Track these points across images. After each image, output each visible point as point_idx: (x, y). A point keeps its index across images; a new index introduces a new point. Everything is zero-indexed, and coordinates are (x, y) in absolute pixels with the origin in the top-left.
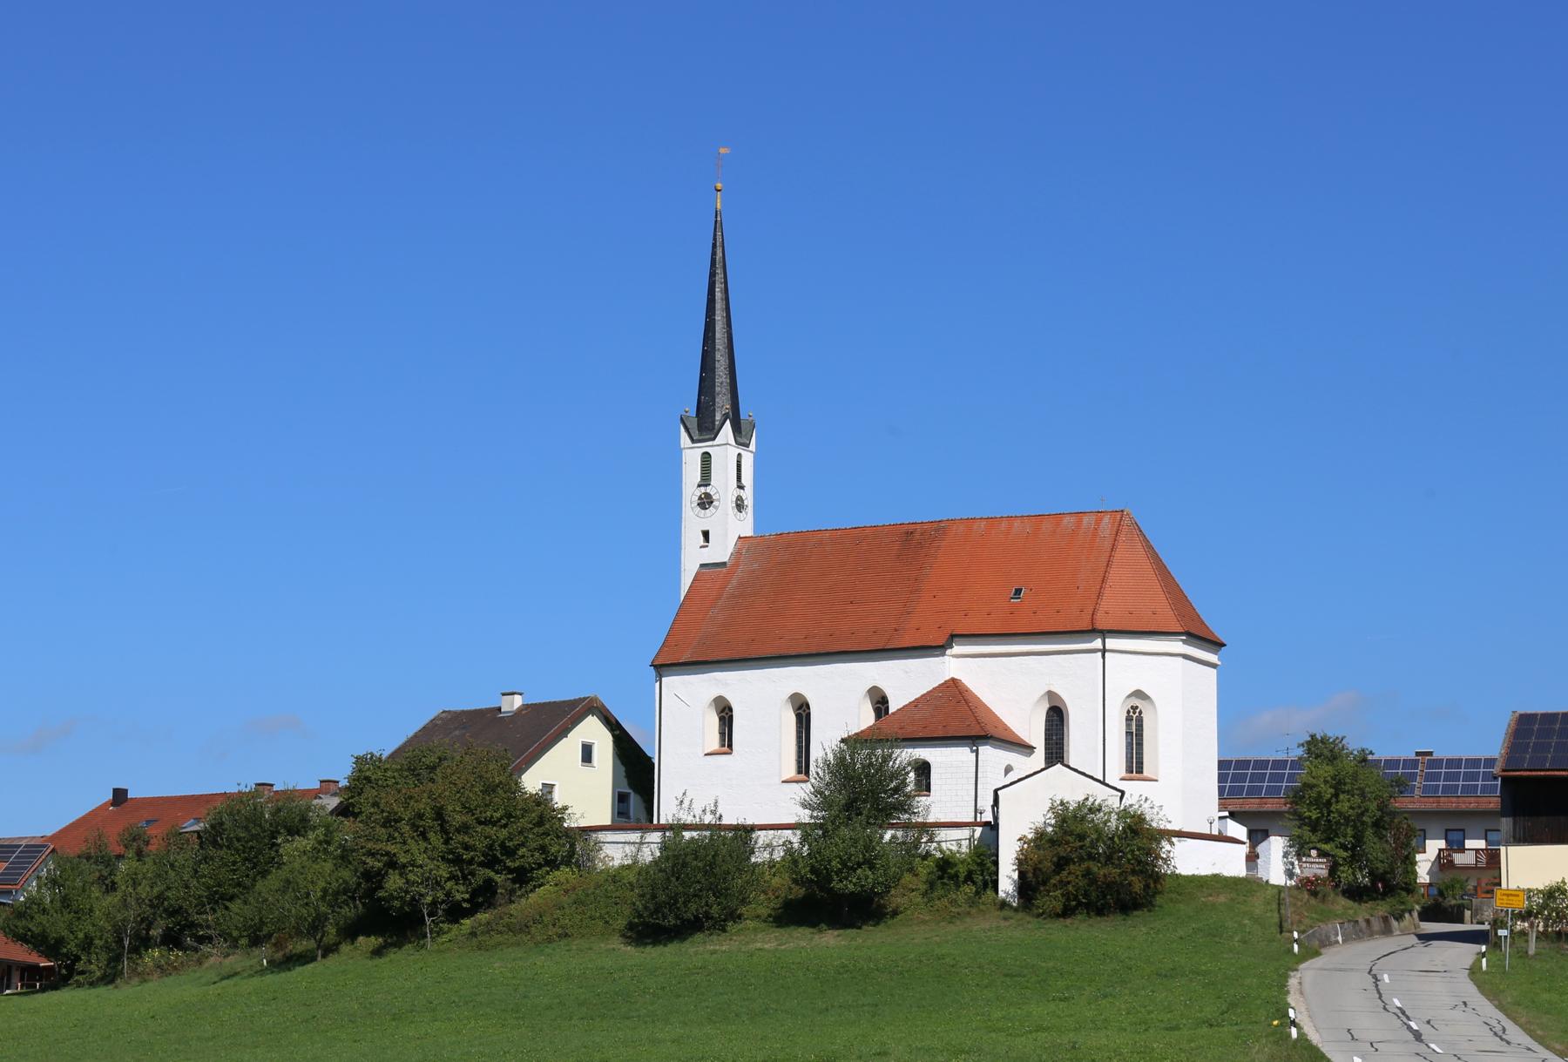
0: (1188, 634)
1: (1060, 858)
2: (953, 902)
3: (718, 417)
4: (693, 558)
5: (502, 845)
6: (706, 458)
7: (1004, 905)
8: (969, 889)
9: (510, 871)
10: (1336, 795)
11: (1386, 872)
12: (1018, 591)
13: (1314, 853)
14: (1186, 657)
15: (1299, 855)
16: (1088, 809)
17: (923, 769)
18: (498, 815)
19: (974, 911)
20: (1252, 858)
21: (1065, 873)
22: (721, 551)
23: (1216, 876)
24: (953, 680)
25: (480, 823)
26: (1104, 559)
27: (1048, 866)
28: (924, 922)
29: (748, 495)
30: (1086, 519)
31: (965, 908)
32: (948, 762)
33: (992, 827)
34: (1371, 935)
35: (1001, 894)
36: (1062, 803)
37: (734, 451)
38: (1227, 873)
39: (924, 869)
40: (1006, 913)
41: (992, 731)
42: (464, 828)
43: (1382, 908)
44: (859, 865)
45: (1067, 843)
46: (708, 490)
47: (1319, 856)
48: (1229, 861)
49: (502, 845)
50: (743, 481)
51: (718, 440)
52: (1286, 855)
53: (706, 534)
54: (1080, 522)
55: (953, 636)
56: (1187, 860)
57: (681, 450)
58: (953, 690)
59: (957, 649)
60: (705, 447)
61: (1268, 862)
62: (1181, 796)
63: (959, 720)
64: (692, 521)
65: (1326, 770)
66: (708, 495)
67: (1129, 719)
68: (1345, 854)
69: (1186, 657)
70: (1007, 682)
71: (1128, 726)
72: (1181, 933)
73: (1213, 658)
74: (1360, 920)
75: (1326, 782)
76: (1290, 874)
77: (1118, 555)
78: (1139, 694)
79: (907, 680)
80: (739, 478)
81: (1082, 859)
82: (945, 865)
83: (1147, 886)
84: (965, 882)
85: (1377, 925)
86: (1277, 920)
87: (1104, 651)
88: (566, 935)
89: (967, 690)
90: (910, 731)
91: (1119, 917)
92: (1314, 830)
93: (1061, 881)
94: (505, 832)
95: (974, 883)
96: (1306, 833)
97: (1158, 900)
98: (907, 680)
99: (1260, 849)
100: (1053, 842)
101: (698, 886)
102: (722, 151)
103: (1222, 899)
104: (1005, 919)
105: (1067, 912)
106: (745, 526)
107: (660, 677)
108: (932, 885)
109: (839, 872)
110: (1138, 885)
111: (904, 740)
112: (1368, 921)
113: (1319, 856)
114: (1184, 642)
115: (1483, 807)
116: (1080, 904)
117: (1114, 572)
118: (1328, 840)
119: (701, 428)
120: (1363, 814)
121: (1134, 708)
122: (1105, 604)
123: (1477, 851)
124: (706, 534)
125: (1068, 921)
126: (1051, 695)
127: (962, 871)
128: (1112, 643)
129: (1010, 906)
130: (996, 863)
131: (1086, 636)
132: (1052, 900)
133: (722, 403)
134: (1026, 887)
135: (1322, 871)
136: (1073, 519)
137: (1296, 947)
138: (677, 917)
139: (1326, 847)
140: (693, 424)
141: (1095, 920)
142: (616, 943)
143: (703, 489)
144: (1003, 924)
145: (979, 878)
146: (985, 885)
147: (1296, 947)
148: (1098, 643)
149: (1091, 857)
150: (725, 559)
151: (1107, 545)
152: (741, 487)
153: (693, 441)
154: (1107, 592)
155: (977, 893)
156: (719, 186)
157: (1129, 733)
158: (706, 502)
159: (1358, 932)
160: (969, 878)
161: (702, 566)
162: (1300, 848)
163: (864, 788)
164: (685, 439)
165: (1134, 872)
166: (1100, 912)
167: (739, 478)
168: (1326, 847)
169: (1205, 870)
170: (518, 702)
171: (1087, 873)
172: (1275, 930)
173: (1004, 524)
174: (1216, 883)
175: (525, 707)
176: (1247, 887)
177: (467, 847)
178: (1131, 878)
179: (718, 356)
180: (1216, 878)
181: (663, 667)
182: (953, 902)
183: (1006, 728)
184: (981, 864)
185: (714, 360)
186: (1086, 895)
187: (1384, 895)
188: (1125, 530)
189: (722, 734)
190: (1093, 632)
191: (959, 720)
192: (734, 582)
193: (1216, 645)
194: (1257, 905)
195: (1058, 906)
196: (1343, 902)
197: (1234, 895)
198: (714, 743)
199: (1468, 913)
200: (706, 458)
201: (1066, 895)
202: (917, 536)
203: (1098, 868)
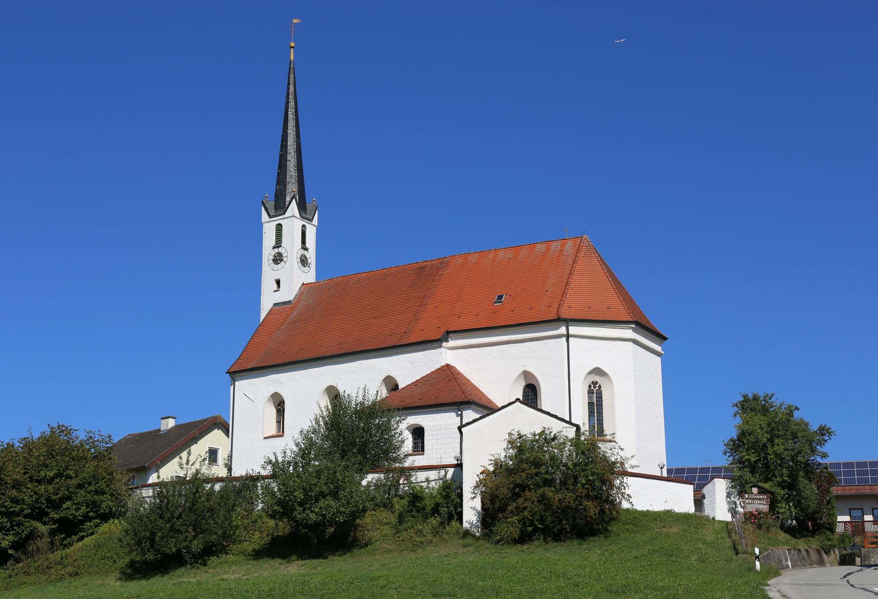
0: (637, 323)
1: (517, 485)
2: (419, 532)
3: (288, 199)
4: (269, 299)
5: (48, 500)
6: (279, 228)
7: (467, 533)
8: (434, 521)
9: (55, 521)
10: (771, 440)
11: (815, 512)
12: (500, 297)
13: (755, 490)
14: (635, 342)
15: (741, 494)
16: (546, 439)
17: (418, 433)
18: (52, 474)
19: (435, 540)
20: (699, 502)
21: (521, 500)
22: (288, 293)
23: (668, 511)
24: (448, 365)
25: (31, 481)
26: (568, 270)
27: (504, 492)
28: (389, 551)
29: (311, 255)
30: (553, 246)
31: (430, 537)
32: (439, 426)
33: (459, 466)
34: (811, 564)
35: (466, 525)
36: (520, 437)
37: (299, 223)
38: (677, 510)
39: (399, 505)
40: (468, 541)
41: (473, 398)
42: (17, 485)
43: (814, 543)
44: (323, 495)
45: (523, 470)
46: (280, 250)
47: (759, 493)
48: (679, 498)
49: (48, 500)
50: (307, 245)
51: (288, 214)
52: (729, 495)
53: (278, 282)
54: (549, 247)
55: (448, 333)
56: (644, 496)
57: (262, 224)
58: (448, 373)
59: (452, 343)
60: (278, 220)
61: (713, 501)
62: (637, 435)
63: (451, 394)
64: (269, 273)
65: (760, 420)
66: (280, 254)
67: (590, 392)
68: (782, 492)
69: (635, 342)
70: (489, 364)
71: (590, 397)
72: (635, 553)
73: (658, 348)
74: (802, 550)
75: (762, 428)
76: (733, 511)
77: (578, 267)
78: (597, 371)
79: (410, 368)
80: (303, 242)
81: (538, 486)
82: (416, 498)
83: (602, 511)
84: (432, 514)
85: (814, 556)
86: (730, 544)
87: (568, 336)
88: (77, 574)
89: (459, 373)
90: (409, 402)
91: (576, 542)
92: (753, 472)
93: (517, 508)
94: (50, 488)
95: (440, 514)
96: (747, 475)
97: (614, 528)
98: (410, 368)
99: (706, 490)
100: (510, 471)
101: (197, 526)
102: (295, 21)
103: (675, 530)
104: (465, 546)
105: (523, 539)
106: (310, 276)
107: (234, 381)
108: (401, 519)
109: (301, 504)
110: (592, 509)
111: (398, 409)
112: (807, 551)
113: (759, 493)
114: (634, 330)
115: (847, 493)
116: (536, 529)
117: (575, 280)
118: (767, 480)
119: (277, 208)
120: (796, 455)
121: (595, 383)
122: (569, 300)
123: (845, 522)
124: (278, 282)
125: (525, 547)
126: (526, 374)
127: (429, 504)
128: (573, 330)
129: (474, 536)
130: (460, 496)
131: (553, 325)
132: (509, 526)
133: (292, 187)
134: (488, 517)
135: (765, 507)
136: (543, 246)
137: (758, 564)
138: (158, 551)
139: (767, 486)
140: (271, 205)
141: (552, 545)
142: (113, 583)
143: (276, 250)
144: (461, 550)
145: (443, 510)
146: (450, 517)
147: (758, 564)
148: (563, 330)
149: (549, 483)
150: (291, 298)
151: (570, 260)
152: (305, 249)
153: (270, 216)
154: (569, 292)
155: (442, 523)
156: (292, 44)
157: (591, 404)
158: (278, 259)
159: (803, 561)
160: (436, 510)
161: (275, 304)
162: (740, 488)
163: (355, 436)
164: (265, 216)
165: (588, 497)
166: (557, 538)
167: (303, 242)
168: (767, 486)
169: (658, 507)
170: (171, 423)
171: (543, 498)
172: (731, 552)
173: (492, 255)
174: (668, 517)
175: (177, 427)
176: (697, 520)
177: (15, 501)
178: (585, 503)
179: (289, 157)
180: (669, 513)
181: (235, 374)
182: (419, 532)
183: (490, 402)
184: (447, 497)
185: (286, 160)
186: (542, 520)
187: (813, 533)
188: (584, 249)
189: (278, 422)
190: (559, 320)
191: (451, 394)
192: (295, 313)
193: (660, 337)
194: (709, 535)
195: (516, 532)
196: (783, 536)
197: (685, 527)
198: (273, 430)
199: (858, 560)
200: (279, 228)
201: (522, 521)
202: (427, 269)
203: (558, 494)
